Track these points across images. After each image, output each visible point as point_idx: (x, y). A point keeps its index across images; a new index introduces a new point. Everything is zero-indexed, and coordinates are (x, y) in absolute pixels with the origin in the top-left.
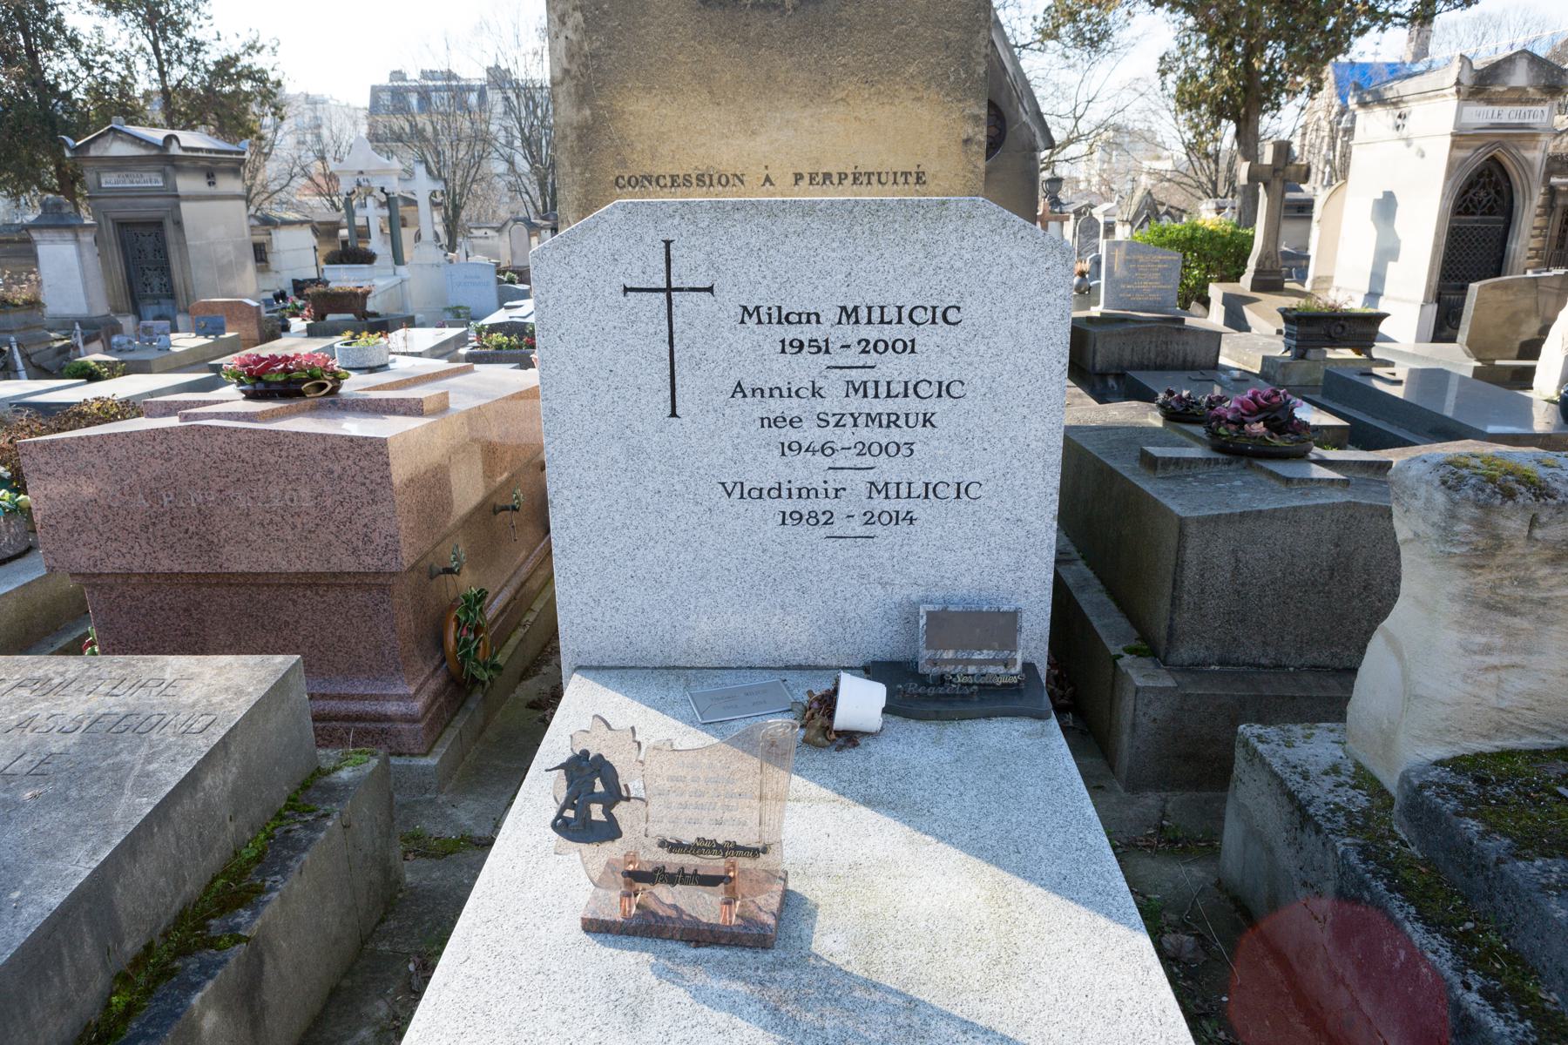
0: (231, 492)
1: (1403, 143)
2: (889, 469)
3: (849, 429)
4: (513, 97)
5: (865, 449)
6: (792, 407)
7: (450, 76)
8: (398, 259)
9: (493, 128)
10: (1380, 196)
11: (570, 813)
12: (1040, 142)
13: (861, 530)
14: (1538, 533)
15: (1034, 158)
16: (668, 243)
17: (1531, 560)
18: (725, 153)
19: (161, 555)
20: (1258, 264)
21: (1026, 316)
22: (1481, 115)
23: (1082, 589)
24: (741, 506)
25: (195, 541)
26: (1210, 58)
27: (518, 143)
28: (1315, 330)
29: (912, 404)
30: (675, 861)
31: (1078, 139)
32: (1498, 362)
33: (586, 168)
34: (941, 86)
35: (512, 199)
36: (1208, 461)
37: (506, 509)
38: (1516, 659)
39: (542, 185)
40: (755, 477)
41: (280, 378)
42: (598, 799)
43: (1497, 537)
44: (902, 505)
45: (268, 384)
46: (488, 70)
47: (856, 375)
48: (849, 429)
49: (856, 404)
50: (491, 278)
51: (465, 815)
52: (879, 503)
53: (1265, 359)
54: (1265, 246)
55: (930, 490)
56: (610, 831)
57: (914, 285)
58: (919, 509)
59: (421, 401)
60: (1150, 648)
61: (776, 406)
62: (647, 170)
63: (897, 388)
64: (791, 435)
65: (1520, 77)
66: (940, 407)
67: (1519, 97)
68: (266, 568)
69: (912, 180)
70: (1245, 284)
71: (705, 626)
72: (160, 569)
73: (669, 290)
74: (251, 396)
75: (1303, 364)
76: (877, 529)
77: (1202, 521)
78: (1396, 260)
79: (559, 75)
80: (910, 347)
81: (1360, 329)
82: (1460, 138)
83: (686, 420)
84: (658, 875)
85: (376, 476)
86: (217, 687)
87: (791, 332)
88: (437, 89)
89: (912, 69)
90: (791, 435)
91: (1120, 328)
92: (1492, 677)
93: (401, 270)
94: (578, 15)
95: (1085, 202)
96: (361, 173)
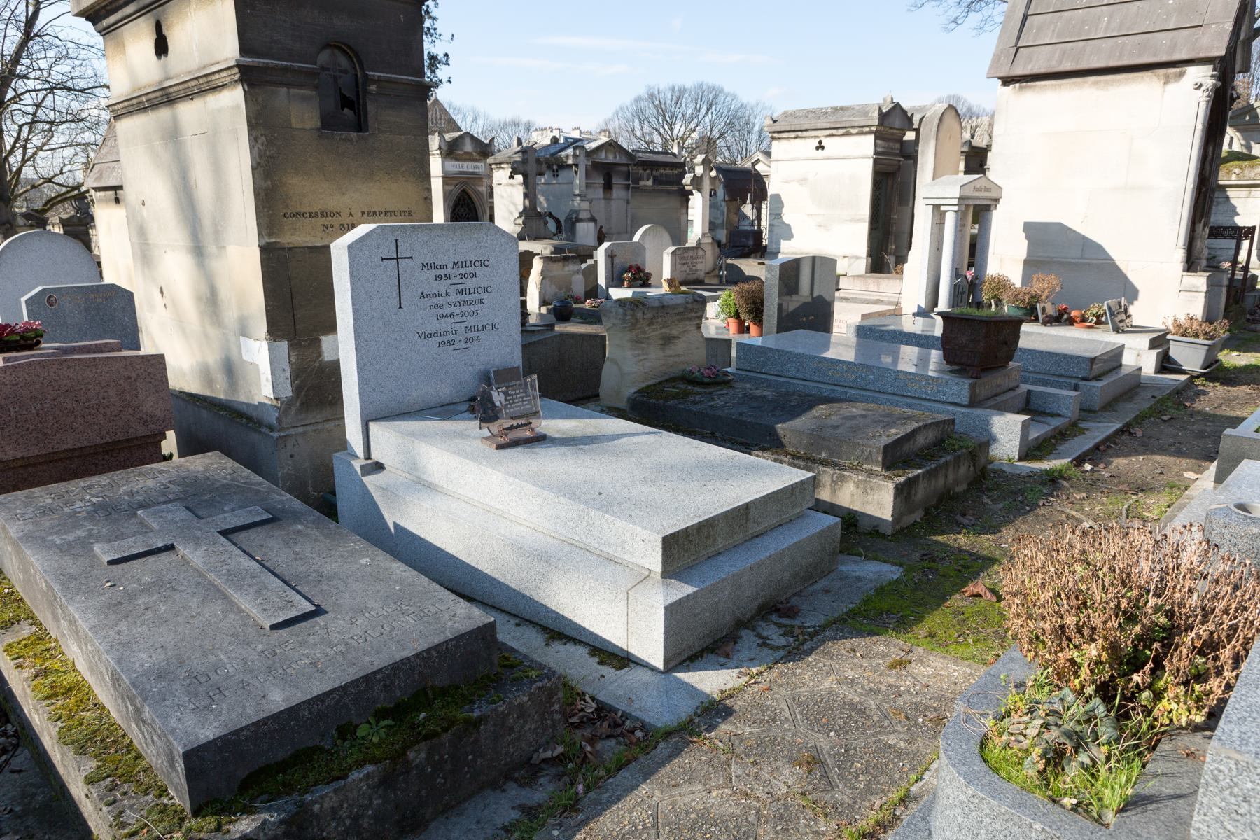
2: (471, 321)
6: (439, 300)
19: (7, 448)
24: (425, 341)
25: (34, 435)
29: (477, 296)
40: (430, 329)
47: (459, 287)
49: (460, 298)
52: (469, 335)
61: (435, 301)
64: (440, 311)
65: (468, 147)
67: (469, 158)
68: (85, 443)
80: (475, 275)
87: (439, 272)
90: (440, 311)
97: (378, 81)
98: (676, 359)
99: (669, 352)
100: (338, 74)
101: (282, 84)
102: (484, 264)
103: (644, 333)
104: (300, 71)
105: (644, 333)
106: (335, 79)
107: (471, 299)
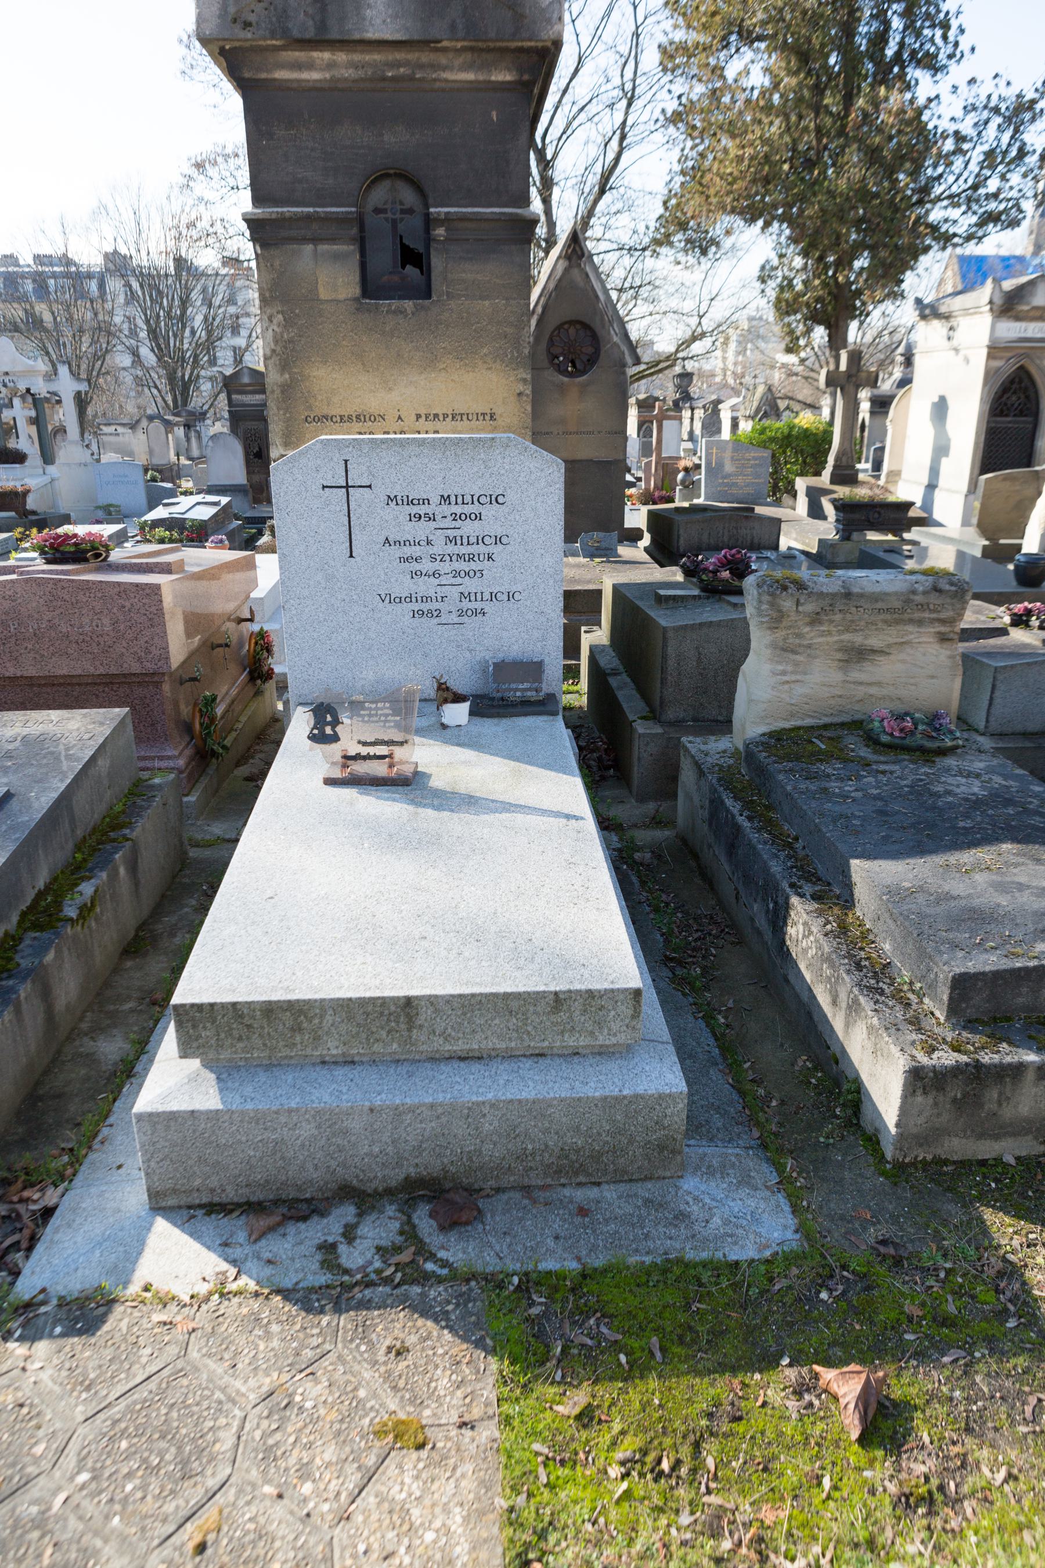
0: (56, 621)
1: (953, 353)
2: (470, 585)
3: (448, 563)
4: (135, 285)
5: (457, 574)
6: (416, 551)
7: (66, 260)
8: (48, 458)
9: (118, 319)
10: (936, 400)
11: (316, 732)
12: (629, 360)
13: (456, 620)
14: (800, 608)
15: (624, 373)
16: (346, 461)
17: (800, 623)
18: (374, 401)
19: (8, 665)
20: (837, 459)
21: (540, 499)
22: (1011, 330)
23: (620, 688)
24: (390, 607)
25: (32, 655)
26: (805, 268)
27: (143, 335)
28: (857, 516)
29: (481, 549)
30: (364, 751)
31: (703, 335)
32: (1002, 541)
33: (286, 410)
34: (503, 361)
35: (140, 394)
36: (699, 597)
37: (220, 646)
38: (798, 677)
39: (171, 378)
41: (72, 549)
42: (329, 724)
43: (780, 611)
44: (478, 605)
45: (63, 553)
46: (106, 256)
48: (448, 563)
49: (451, 549)
50: (138, 477)
51: (217, 829)
52: (466, 604)
53: (820, 541)
54: (842, 443)
55: (493, 596)
56: (335, 738)
57: (479, 483)
58: (488, 607)
59: (169, 564)
60: (653, 715)
61: (408, 551)
62: (325, 412)
63: (473, 540)
64: (416, 567)
66: (496, 550)
68: (79, 672)
69: (488, 418)
70: (825, 478)
71: (371, 676)
72: (7, 674)
73: (347, 487)
74: (49, 562)
75: (848, 545)
76: (465, 619)
77: (674, 628)
78: (947, 455)
79: (268, 353)
80: (479, 517)
81: (896, 516)
82: (994, 350)
83: (358, 559)
84: (357, 757)
85: (153, 609)
86: (78, 731)
88: (54, 275)
89: (485, 351)
90: (416, 567)
91: (699, 516)
92: (786, 687)
93: (51, 469)
94: (280, 316)
95: (714, 397)
96: (7, 374)
97: (447, 221)
98: (873, 690)
99: (855, 675)
100: (398, 216)
101: (305, 240)
102: (496, 500)
103: (799, 636)
104: (327, 219)
105: (799, 636)
106: (394, 222)
107: (472, 554)
